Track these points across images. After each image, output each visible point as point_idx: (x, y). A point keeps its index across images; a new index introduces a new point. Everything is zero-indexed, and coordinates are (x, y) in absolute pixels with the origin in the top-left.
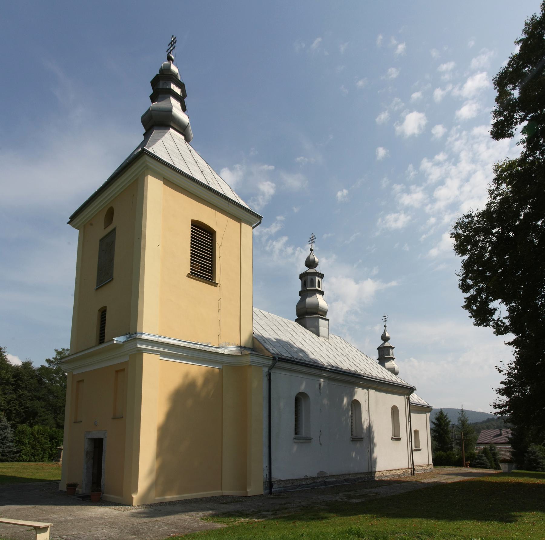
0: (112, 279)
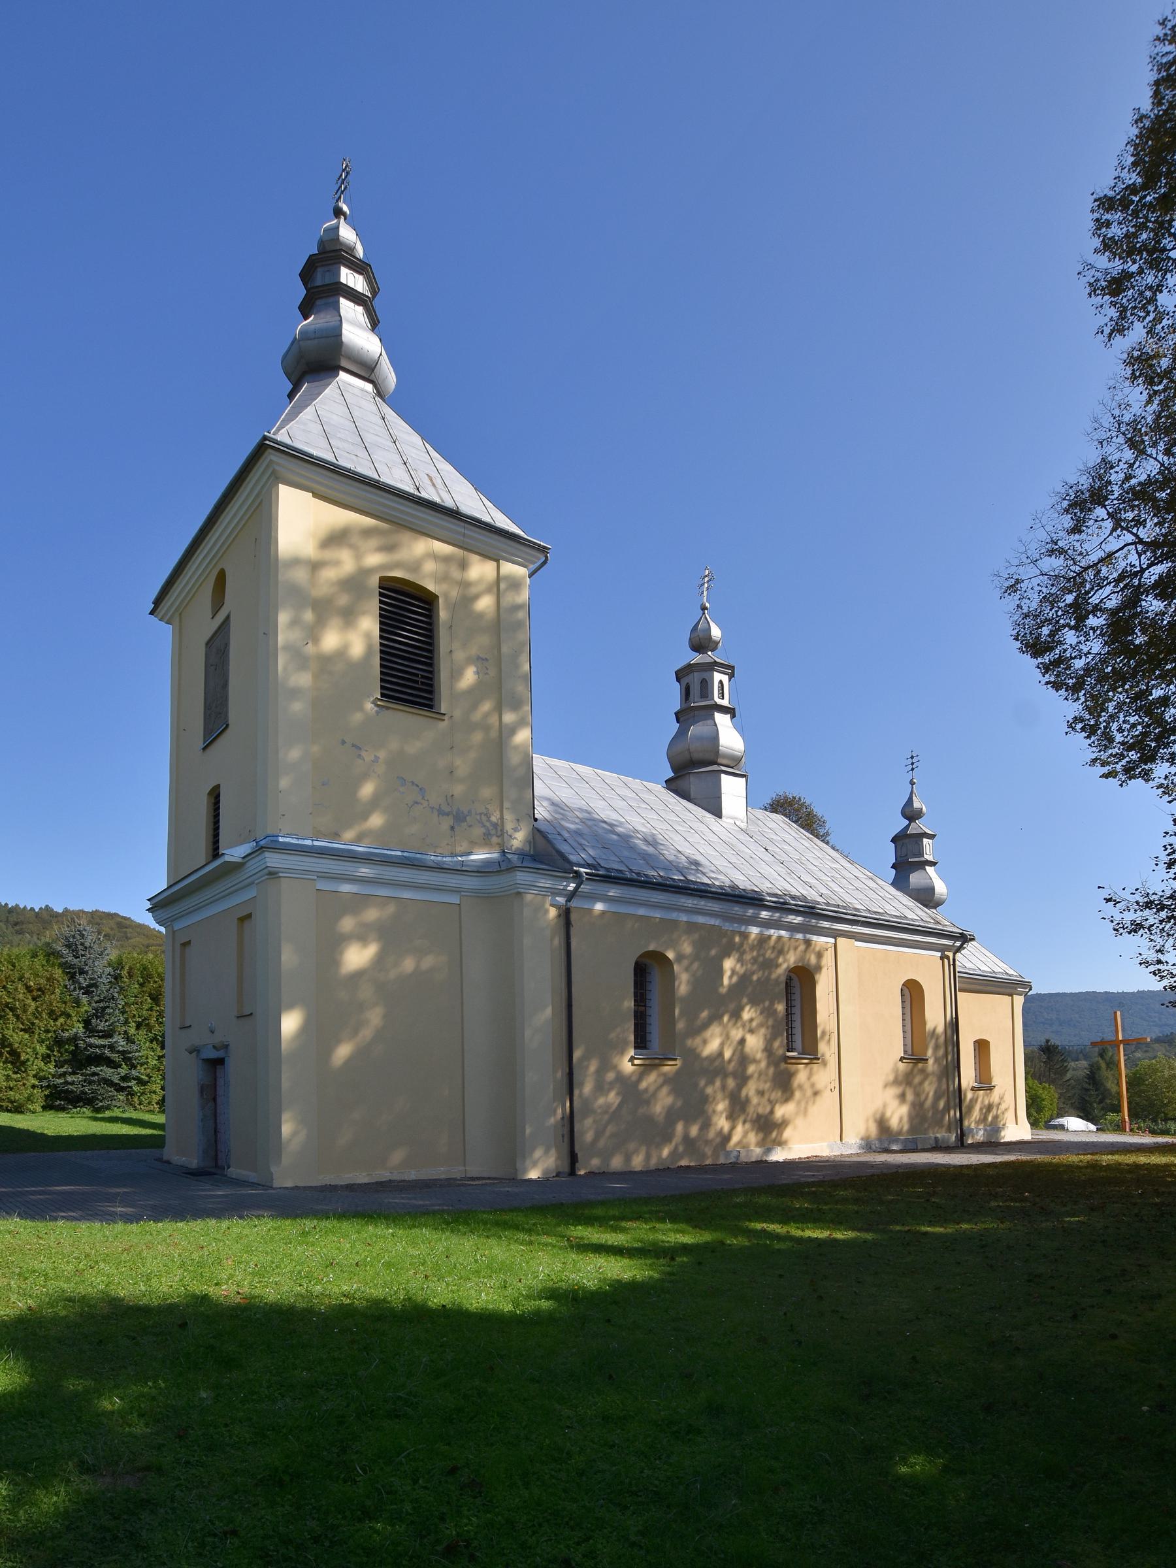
0: (227, 726)
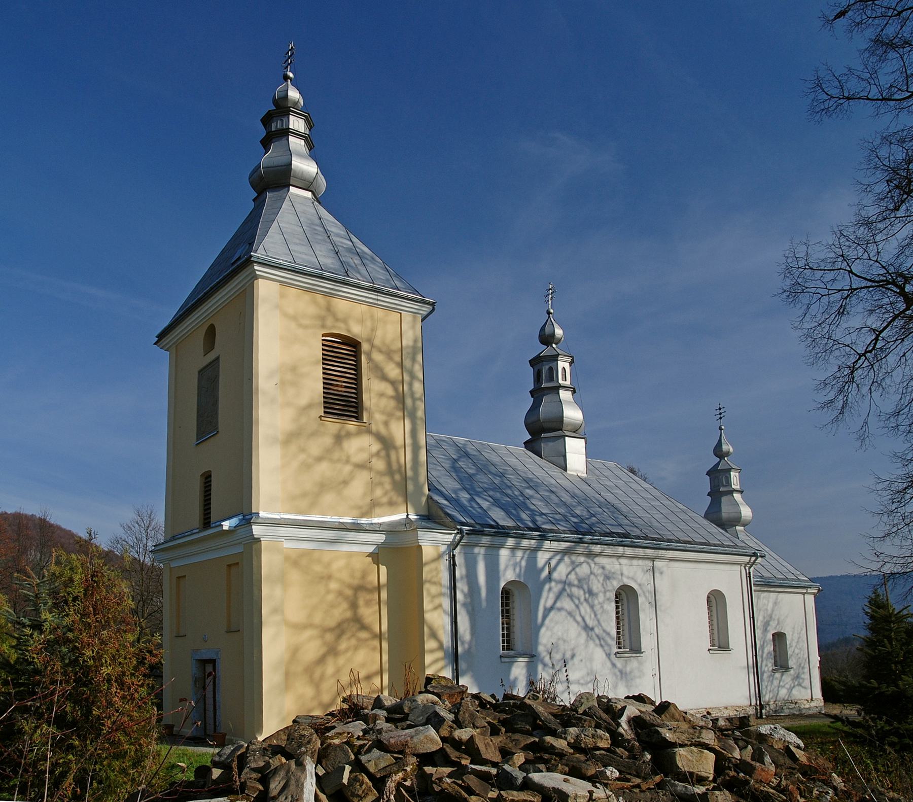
0: (218, 432)
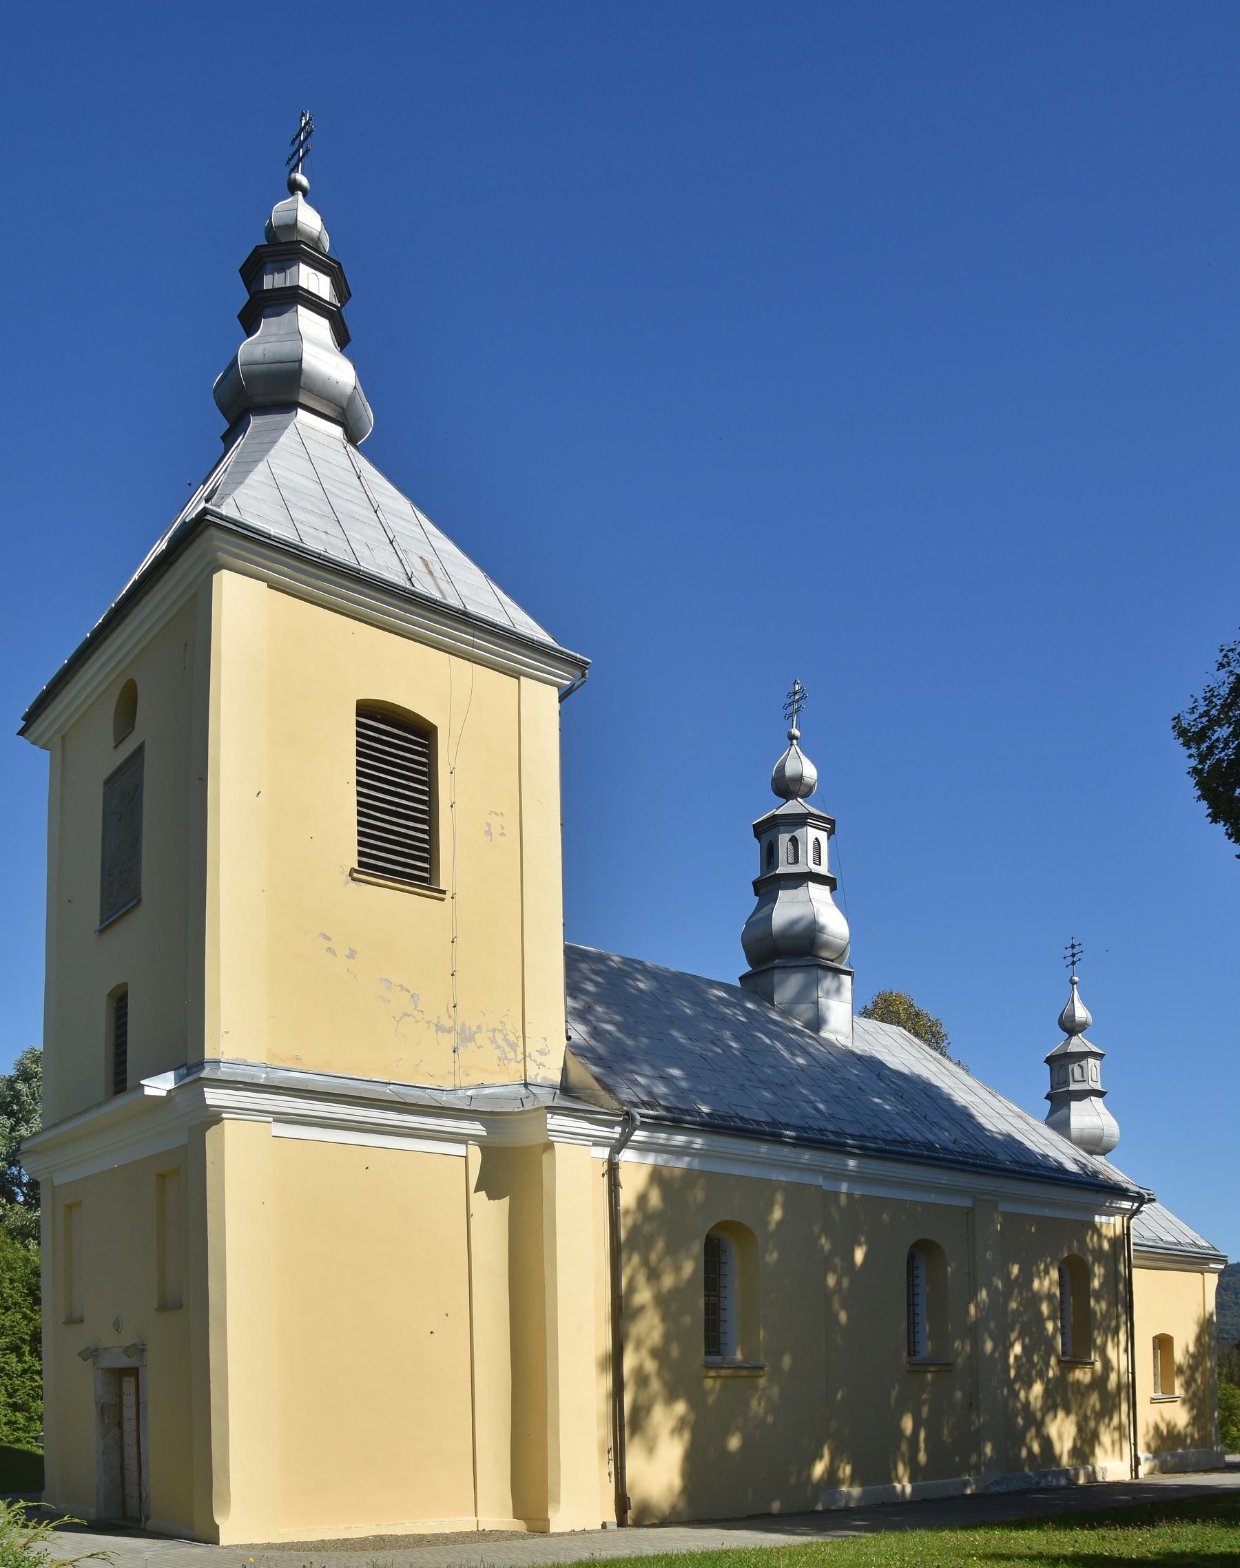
0: (139, 901)
